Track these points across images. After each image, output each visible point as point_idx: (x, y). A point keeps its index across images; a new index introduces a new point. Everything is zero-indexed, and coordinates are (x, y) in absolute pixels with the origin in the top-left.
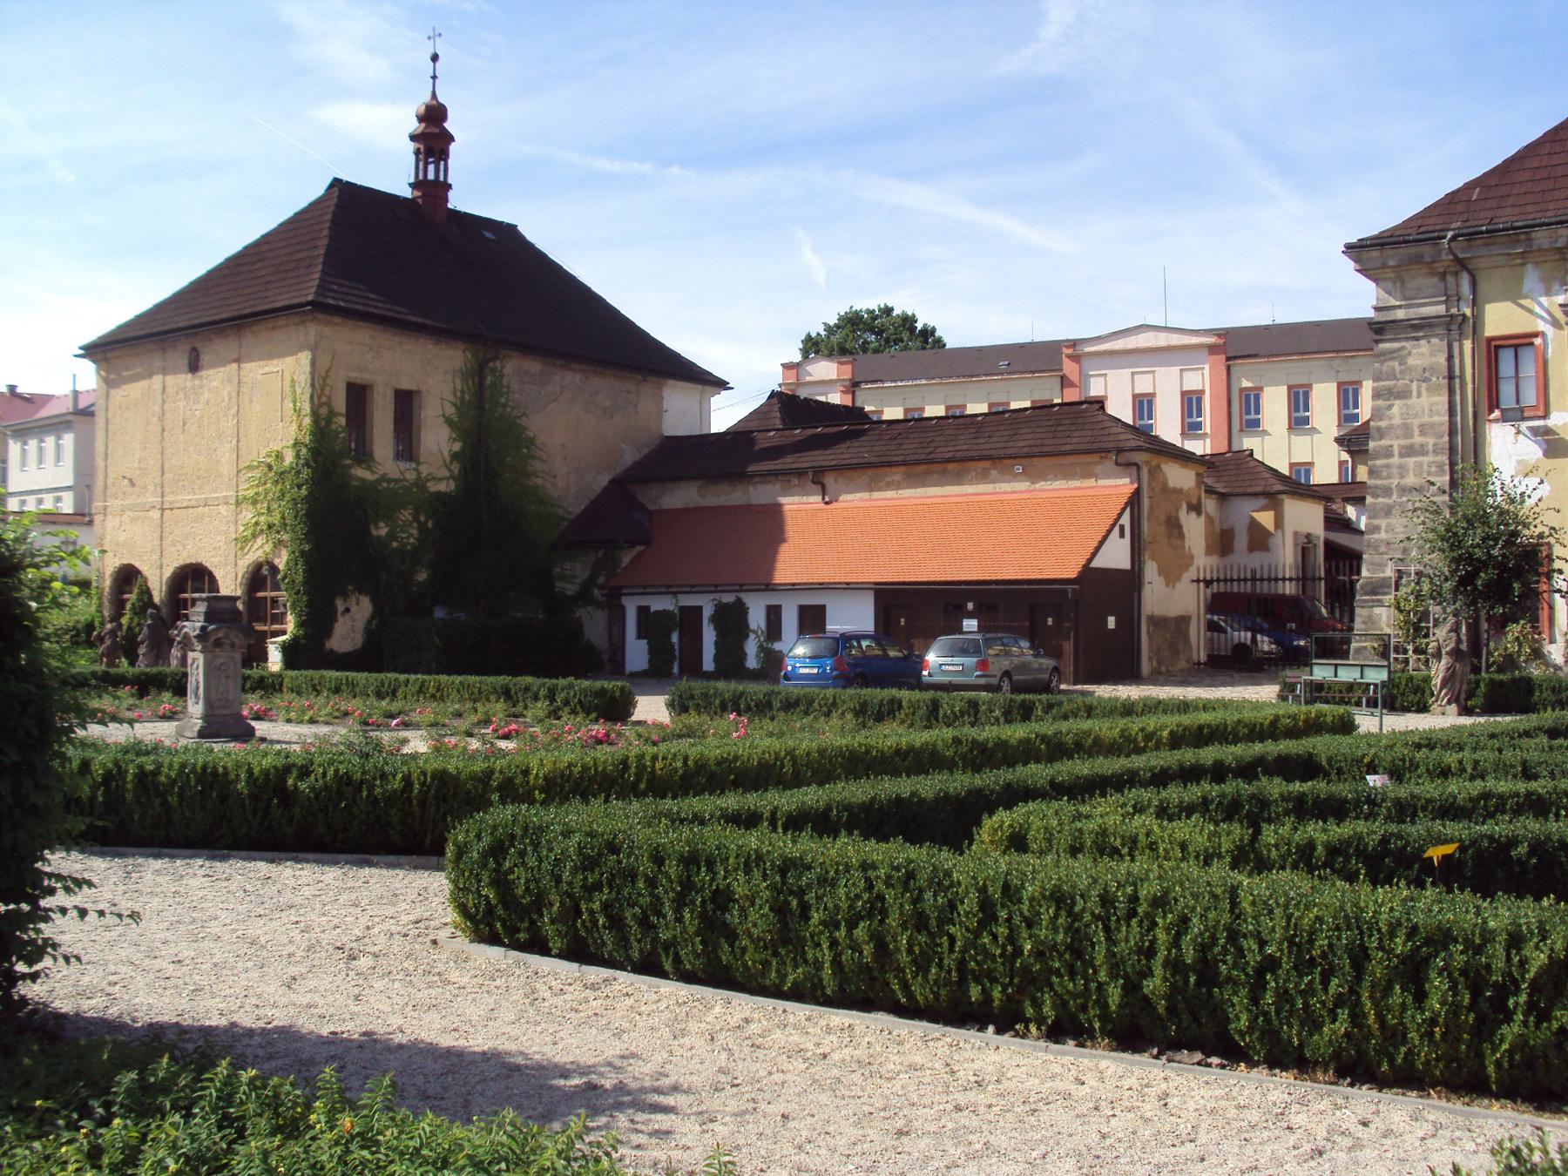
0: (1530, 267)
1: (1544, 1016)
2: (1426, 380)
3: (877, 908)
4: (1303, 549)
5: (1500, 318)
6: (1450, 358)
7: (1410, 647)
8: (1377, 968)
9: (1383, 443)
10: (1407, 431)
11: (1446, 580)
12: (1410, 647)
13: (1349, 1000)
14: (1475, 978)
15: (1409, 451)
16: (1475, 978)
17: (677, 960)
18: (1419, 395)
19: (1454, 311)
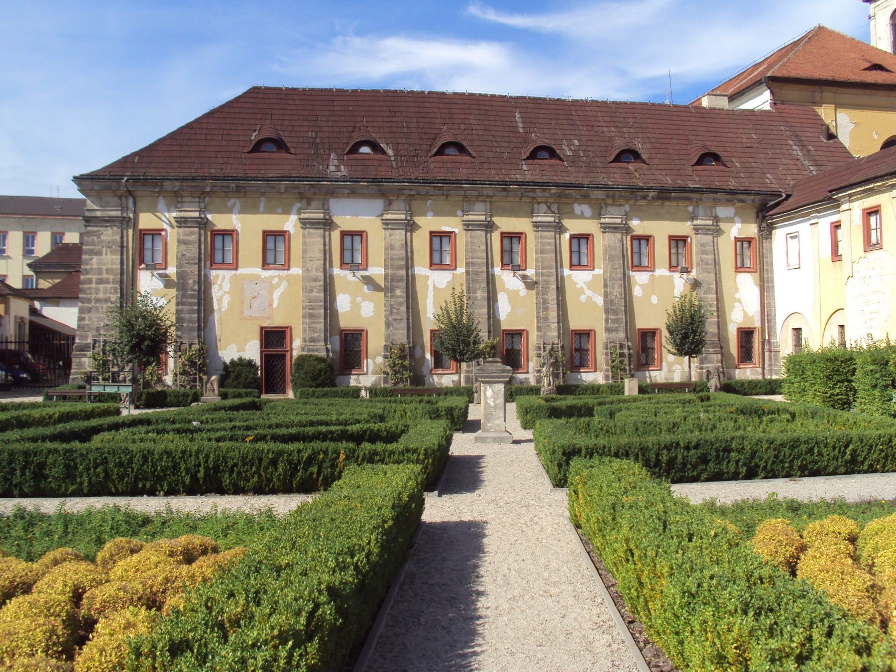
0: (161, 198)
1: (306, 470)
2: (110, 247)
3: (105, 461)
4: (20, 325)
5: (146, 221)
6: (122, 237)
7: (100, 378)
8: (264, 463)
9: (88, 276)
10: (100, 271)
11: (126, 345)
12: (100, 378)
13: (257, 472)
14: (290, 462)
15: (100, 281)
16: (290, 462)
17: (21, 489)
18: (106, 254)
19: (125, 215)
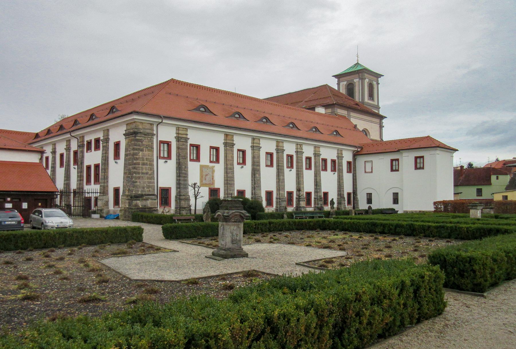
15: (144, 164)
